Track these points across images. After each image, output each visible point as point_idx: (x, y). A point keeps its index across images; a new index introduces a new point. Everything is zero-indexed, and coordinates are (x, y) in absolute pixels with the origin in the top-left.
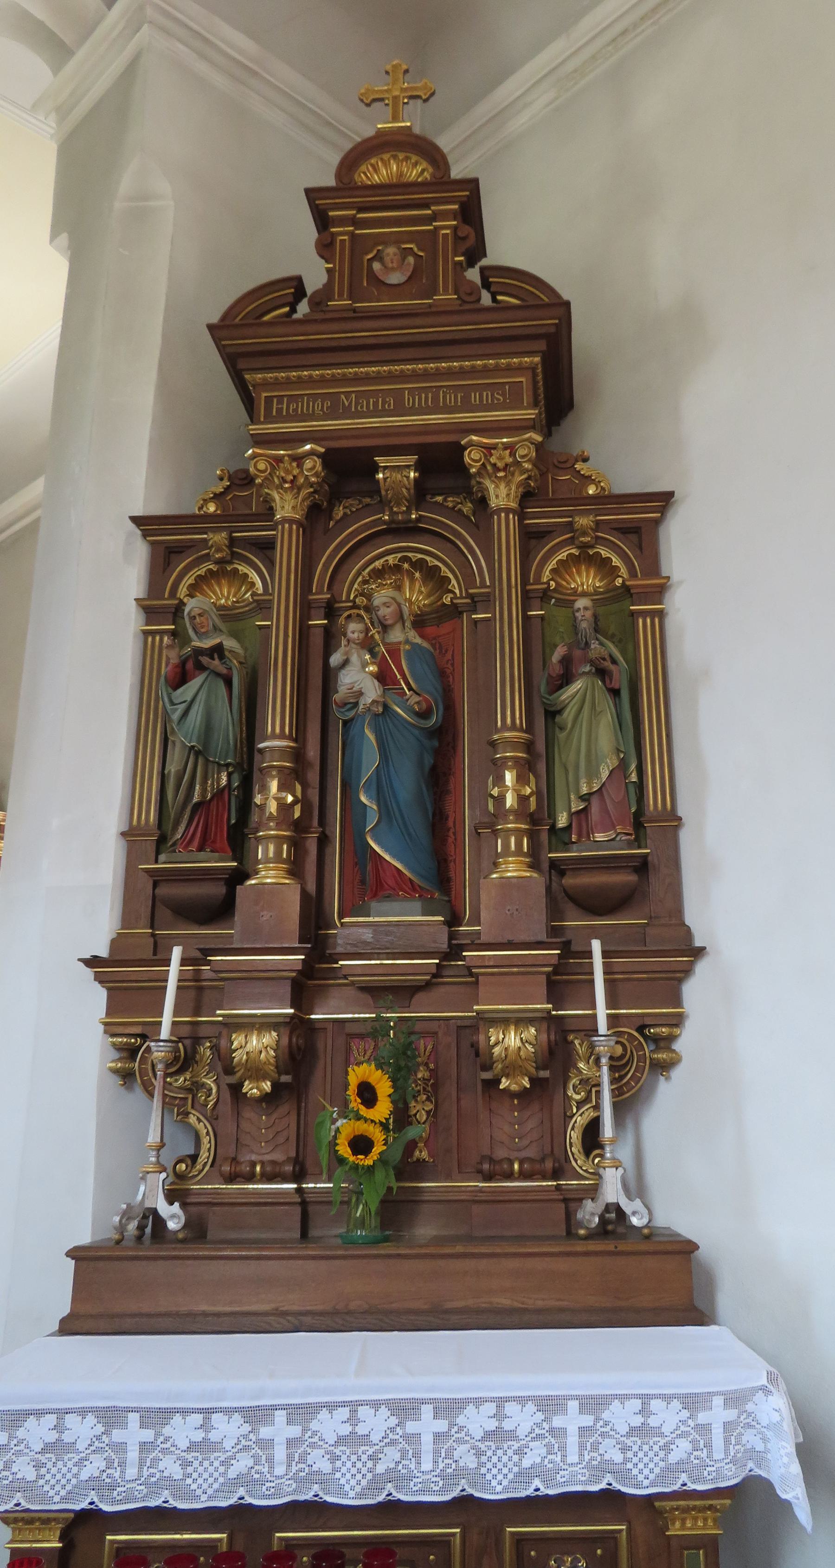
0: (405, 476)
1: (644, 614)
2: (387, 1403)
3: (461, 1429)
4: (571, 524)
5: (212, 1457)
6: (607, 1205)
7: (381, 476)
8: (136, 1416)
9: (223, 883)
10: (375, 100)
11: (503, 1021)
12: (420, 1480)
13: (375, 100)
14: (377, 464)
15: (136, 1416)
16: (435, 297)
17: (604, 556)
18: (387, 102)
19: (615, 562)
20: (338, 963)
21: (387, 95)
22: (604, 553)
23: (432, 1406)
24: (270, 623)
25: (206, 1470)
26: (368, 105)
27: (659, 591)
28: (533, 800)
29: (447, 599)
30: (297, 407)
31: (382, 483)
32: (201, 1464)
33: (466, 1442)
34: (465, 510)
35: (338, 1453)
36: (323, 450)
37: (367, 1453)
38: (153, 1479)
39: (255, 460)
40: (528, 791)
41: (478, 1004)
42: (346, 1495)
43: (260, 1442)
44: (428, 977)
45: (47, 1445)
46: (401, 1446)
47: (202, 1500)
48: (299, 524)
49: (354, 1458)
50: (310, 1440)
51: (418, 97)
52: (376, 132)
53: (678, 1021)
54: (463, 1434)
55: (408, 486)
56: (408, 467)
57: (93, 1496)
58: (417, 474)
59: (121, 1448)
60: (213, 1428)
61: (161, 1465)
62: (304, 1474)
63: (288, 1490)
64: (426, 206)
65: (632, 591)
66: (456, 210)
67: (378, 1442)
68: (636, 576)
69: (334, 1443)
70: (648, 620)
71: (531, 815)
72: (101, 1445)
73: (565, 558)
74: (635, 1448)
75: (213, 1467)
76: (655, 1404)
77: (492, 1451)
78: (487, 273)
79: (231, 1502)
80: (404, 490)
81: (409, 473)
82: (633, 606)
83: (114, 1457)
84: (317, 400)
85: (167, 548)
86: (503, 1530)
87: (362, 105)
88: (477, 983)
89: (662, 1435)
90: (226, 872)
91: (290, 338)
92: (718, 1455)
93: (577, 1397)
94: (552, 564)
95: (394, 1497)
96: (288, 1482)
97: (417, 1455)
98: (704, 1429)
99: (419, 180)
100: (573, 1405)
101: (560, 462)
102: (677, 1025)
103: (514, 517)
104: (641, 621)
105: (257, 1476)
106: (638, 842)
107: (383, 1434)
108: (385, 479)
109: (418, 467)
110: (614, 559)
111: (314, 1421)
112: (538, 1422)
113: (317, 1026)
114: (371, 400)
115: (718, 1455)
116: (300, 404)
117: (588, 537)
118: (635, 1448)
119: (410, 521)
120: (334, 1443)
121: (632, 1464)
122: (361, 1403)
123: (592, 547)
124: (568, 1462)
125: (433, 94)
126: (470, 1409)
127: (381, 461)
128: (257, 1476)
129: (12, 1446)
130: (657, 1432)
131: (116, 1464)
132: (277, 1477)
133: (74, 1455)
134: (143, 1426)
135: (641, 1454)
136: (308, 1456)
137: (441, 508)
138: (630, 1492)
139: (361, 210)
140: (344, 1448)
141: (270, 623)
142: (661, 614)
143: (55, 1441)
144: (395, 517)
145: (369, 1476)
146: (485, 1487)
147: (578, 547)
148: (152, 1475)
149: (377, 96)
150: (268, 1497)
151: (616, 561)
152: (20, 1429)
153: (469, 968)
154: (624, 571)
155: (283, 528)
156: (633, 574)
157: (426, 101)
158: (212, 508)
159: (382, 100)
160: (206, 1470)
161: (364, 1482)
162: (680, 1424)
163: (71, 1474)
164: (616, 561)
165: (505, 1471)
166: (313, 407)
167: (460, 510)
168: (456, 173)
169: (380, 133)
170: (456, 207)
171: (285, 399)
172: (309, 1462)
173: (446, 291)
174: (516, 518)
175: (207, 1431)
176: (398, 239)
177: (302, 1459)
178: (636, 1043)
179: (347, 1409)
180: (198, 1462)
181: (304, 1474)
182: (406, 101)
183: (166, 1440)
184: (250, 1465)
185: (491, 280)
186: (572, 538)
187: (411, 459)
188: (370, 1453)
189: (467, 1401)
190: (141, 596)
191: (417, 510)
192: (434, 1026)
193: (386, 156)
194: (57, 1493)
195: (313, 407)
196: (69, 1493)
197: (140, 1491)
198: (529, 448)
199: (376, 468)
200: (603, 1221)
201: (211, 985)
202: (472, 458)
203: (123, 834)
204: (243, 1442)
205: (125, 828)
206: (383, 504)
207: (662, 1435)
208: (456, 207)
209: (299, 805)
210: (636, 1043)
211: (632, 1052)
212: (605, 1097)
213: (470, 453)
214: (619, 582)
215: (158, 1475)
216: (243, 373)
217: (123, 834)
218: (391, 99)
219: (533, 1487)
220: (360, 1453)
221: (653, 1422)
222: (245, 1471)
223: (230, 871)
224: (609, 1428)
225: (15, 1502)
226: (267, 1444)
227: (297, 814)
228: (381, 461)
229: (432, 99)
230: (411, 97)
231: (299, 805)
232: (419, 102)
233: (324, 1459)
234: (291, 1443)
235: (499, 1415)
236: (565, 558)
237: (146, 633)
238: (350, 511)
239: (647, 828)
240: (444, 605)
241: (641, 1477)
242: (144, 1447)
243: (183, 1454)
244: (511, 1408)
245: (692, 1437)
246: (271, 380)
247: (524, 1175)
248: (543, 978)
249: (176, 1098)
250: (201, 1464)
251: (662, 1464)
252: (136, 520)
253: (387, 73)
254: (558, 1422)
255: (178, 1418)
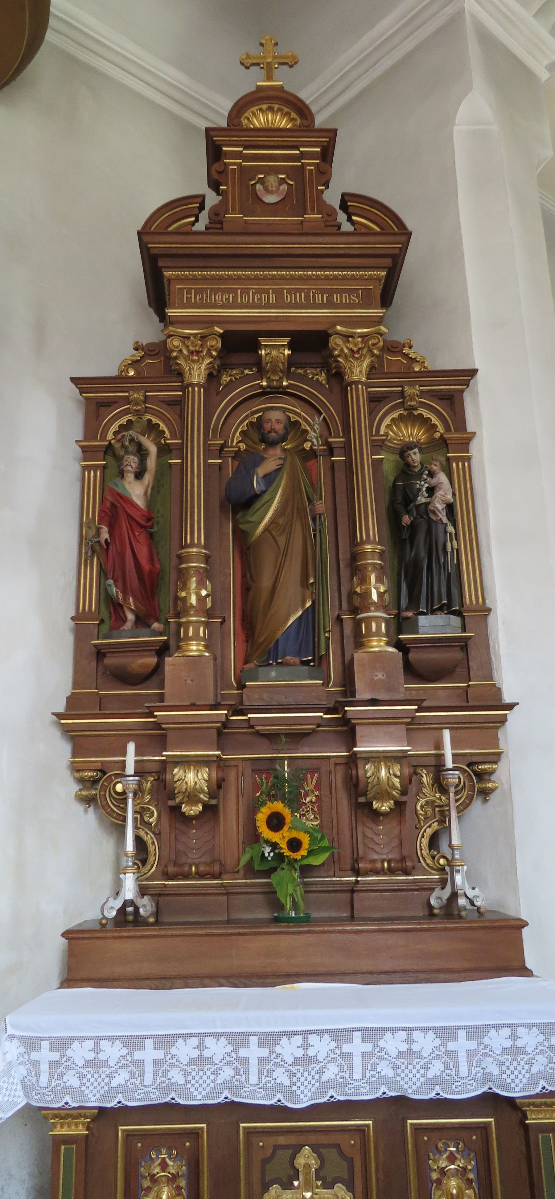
0: (281, 353)
1: (457, 459)
2: (434, 1029)
3: (173, 1056)
4: (402, 392)
5: (101, 1071)
6: (125, 901)
7: (263, 352)
8: (359, 1034)
9: (154, 653)
10: (253, 64)
11: (185, 762)
12: (459, 1084)
13: (253, 64)
14: (261, 343)
15: (151, 1041)
16: (305, 216)
17: (425, 417)
18: (262, 66)
19: (434, 421)
20: (247, 716)
21: (262, 61)
22: (426, 414)
23: (48, 1042)
24: (373, 457)
25: (201, 1078)
26: (247, 68)
27: (465, 443)
28: (209, 600)
29: (307, 446)
30: (203, 296)
31: (263, 358)
32: (92, 1076)
33: (73, 1069)
34: (320, 379)
35: (85, 1073)
36: (222, 331)
37: (420, 1063)
38: (163, 1085)
39: (171, 338)
40: (204, 593)
41: (166, 751)
42: (17, 1104)
43: (343, 1055)
44: (314, 727)
45: (191, 1059)
46: (339, 1062)
47: (516, 1090)
48: (203, 386)
49: (201, 1073)
50: (379, 1054)
51: (286, 64)
52: (256, 88)
53: (495, 758)
54: (174, 1061)
55: (283, 361)
56: (283, 345)
57: (226, 1093)
58: (290, 352)
59: (140, 1063)
60: (309, 1045)
61: (65, 1078)
62: (375, 1079)
63: (48, 1099)
64: (296, 148)
65: (448, 442)
66: (318, 152)
67: (219, 1063)
68: (451, 431)
69: (396, 1056)
70: (460, 464)
71: (208, 610)
72: (543, 1048)
73: (125, 423)
74: (403, 1067)
75: (94, 1079)
76: (416, 1035)
77: (509, 1062)
78: (346, 198)
79: (324, 1100)
80: (281, 365)
81: (284, 350)
82: (171, 460)
83: (135, 1070)
84: (218, 293)
85: (97, 403)
86: (238, 1127)
87: (243, 68)
88: (165, 736)
89: (526, 1053)
90: (157, 644)
91: (242, 246)
92: (357, 1075)
93: (464, 1028)
94: (115, 427)
95: (441, 1096)
96: (153, 1091)
97: (247, 1073)
98: (452, 1054)
99: (288, 127)
100: (45, 1044)
101: (392, 347)
102: (496, 762)
103: (362, 387)
104: (454, 464)
105: (237, 1083)
106: (464, 630)
107: (431, 1051)
108: (266, 355)
109: (290, 346)
110: (433, 419)
111: (173, 1047)
112: (124, 1055)
113: (359, 755)
114: (231, 295)
115: (357, 1075)
116: (205, 295)
117: (414, 402)
118: (403, 1067)
119: (282, 387)
120: (396, 1056)
121: (506, 1075)
122: (206, 1035)
123: (416, 409)
124: (354, 1078)
125: (296, 63)
126: (76, 1045)
127: (264, 341)
128: (237, 1083)
129: (63, 1062)
130: (419, 1055)
131: (137, 1076)
132: (251, 1085)
133: (106, 1069)
134: (468, 1038)
135: (407, 1071)
136: (377, 1066)
137: (303, 378)
138: (415, 1098)
139: (246, 147)
140: (403, 1060)
141: (373, 457)
142: (469, 459)
143: (197, 1056)
144: (271, 384)
145: (527, 1075)
146: (193, 1098)
147: (405, 410)
148: (59, 1085)
149: (255, 61)
150: (459, 1093)
151: (435, 420)
152: (68, 1049)
153: (159, 724)
154: (441, 429)
155: (188, 390)
156: (447, 429)
157: (291, 66)
158: (132, 373)
159: (258, 64)
160: (201, 1078)
161: (524, 1080)
162: (121, 1058)
163: (104, 1083)
164: (435, 420)
165: (204, 1085)
166: (215, 298)
167: (317, 379)
168: (320, 121)
169: (259, 89)
170: (319, 149)
171: (193, 291)
172: (379, 1070)
173: (313, 212)
174: (202, 390)
175: (97, 1053)
176: (276, 170)
177: (374, 1067)
178: (105, 783)
179: (405, 1033)
180: (195, 1072)
181: (375, 1079)
182: (276, 66)
183: (68, 1059)
184: (127, 1078)
185: (349, 204)
186: (403, 403)
187: (285, 341)
188: (108, 1073)
189: (73, 1039)
190: (80, 438)
191: (287, 380)
192: (236, 763)
193: (254, 109)
194: (200, 1093)
195: (215, 298)
196: (207, 1093)
197: (471, 1085)
198: (216, 339)
199: (258, 346)
200: (122, 911)
201: (201, 727)
202: (336, 342)
203: (73, 619)
204: (332, 1056)
205: (73, 614)
206: (261, 372)
207: (526, 1053)
208: (319, 149)
209: (210, 597)
210: (105, 783)
211: (464, 783)
212: (129, 823)
213: (336, 338)
214: (437, 435)
215: (167, 1082)
216: (163, 270)
217: (73, 619)
218: (265, 64)
219: (381, 1091)
220: (100, 1072)
221: (415, 1047)
222: (228, 1079)
223: (161, 644)
224: (175, 1060)
225: (117, 1100)
226: (452, 1054)
227: (209, 605)
228: (264, 341)
229: (295, 66)
230: (280, 64)
231: (210, 597)
232: (287, 67)
233: (389, 1067)
234: (156, 1062)
235: (96, 1049)
236: (125, 423)
237: (84, 468)
238: (235, 378)
239: (466, 617)
240: (304, 449)
241: (90, 1096)
242: (53, 1065)
243: (394, 1060)
244: (209, 1041)
245: (339, 1062)
246: (209, 277)
247: (201, 876)
248: (215, 732)
249: (115, 812)
250: (92, 1076)
251: (422, 1079)
252: (73, 380)
253: (261, 45)
254: (451, 1046)
255: (284, 1040)
